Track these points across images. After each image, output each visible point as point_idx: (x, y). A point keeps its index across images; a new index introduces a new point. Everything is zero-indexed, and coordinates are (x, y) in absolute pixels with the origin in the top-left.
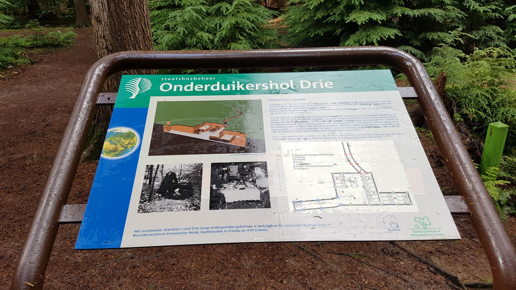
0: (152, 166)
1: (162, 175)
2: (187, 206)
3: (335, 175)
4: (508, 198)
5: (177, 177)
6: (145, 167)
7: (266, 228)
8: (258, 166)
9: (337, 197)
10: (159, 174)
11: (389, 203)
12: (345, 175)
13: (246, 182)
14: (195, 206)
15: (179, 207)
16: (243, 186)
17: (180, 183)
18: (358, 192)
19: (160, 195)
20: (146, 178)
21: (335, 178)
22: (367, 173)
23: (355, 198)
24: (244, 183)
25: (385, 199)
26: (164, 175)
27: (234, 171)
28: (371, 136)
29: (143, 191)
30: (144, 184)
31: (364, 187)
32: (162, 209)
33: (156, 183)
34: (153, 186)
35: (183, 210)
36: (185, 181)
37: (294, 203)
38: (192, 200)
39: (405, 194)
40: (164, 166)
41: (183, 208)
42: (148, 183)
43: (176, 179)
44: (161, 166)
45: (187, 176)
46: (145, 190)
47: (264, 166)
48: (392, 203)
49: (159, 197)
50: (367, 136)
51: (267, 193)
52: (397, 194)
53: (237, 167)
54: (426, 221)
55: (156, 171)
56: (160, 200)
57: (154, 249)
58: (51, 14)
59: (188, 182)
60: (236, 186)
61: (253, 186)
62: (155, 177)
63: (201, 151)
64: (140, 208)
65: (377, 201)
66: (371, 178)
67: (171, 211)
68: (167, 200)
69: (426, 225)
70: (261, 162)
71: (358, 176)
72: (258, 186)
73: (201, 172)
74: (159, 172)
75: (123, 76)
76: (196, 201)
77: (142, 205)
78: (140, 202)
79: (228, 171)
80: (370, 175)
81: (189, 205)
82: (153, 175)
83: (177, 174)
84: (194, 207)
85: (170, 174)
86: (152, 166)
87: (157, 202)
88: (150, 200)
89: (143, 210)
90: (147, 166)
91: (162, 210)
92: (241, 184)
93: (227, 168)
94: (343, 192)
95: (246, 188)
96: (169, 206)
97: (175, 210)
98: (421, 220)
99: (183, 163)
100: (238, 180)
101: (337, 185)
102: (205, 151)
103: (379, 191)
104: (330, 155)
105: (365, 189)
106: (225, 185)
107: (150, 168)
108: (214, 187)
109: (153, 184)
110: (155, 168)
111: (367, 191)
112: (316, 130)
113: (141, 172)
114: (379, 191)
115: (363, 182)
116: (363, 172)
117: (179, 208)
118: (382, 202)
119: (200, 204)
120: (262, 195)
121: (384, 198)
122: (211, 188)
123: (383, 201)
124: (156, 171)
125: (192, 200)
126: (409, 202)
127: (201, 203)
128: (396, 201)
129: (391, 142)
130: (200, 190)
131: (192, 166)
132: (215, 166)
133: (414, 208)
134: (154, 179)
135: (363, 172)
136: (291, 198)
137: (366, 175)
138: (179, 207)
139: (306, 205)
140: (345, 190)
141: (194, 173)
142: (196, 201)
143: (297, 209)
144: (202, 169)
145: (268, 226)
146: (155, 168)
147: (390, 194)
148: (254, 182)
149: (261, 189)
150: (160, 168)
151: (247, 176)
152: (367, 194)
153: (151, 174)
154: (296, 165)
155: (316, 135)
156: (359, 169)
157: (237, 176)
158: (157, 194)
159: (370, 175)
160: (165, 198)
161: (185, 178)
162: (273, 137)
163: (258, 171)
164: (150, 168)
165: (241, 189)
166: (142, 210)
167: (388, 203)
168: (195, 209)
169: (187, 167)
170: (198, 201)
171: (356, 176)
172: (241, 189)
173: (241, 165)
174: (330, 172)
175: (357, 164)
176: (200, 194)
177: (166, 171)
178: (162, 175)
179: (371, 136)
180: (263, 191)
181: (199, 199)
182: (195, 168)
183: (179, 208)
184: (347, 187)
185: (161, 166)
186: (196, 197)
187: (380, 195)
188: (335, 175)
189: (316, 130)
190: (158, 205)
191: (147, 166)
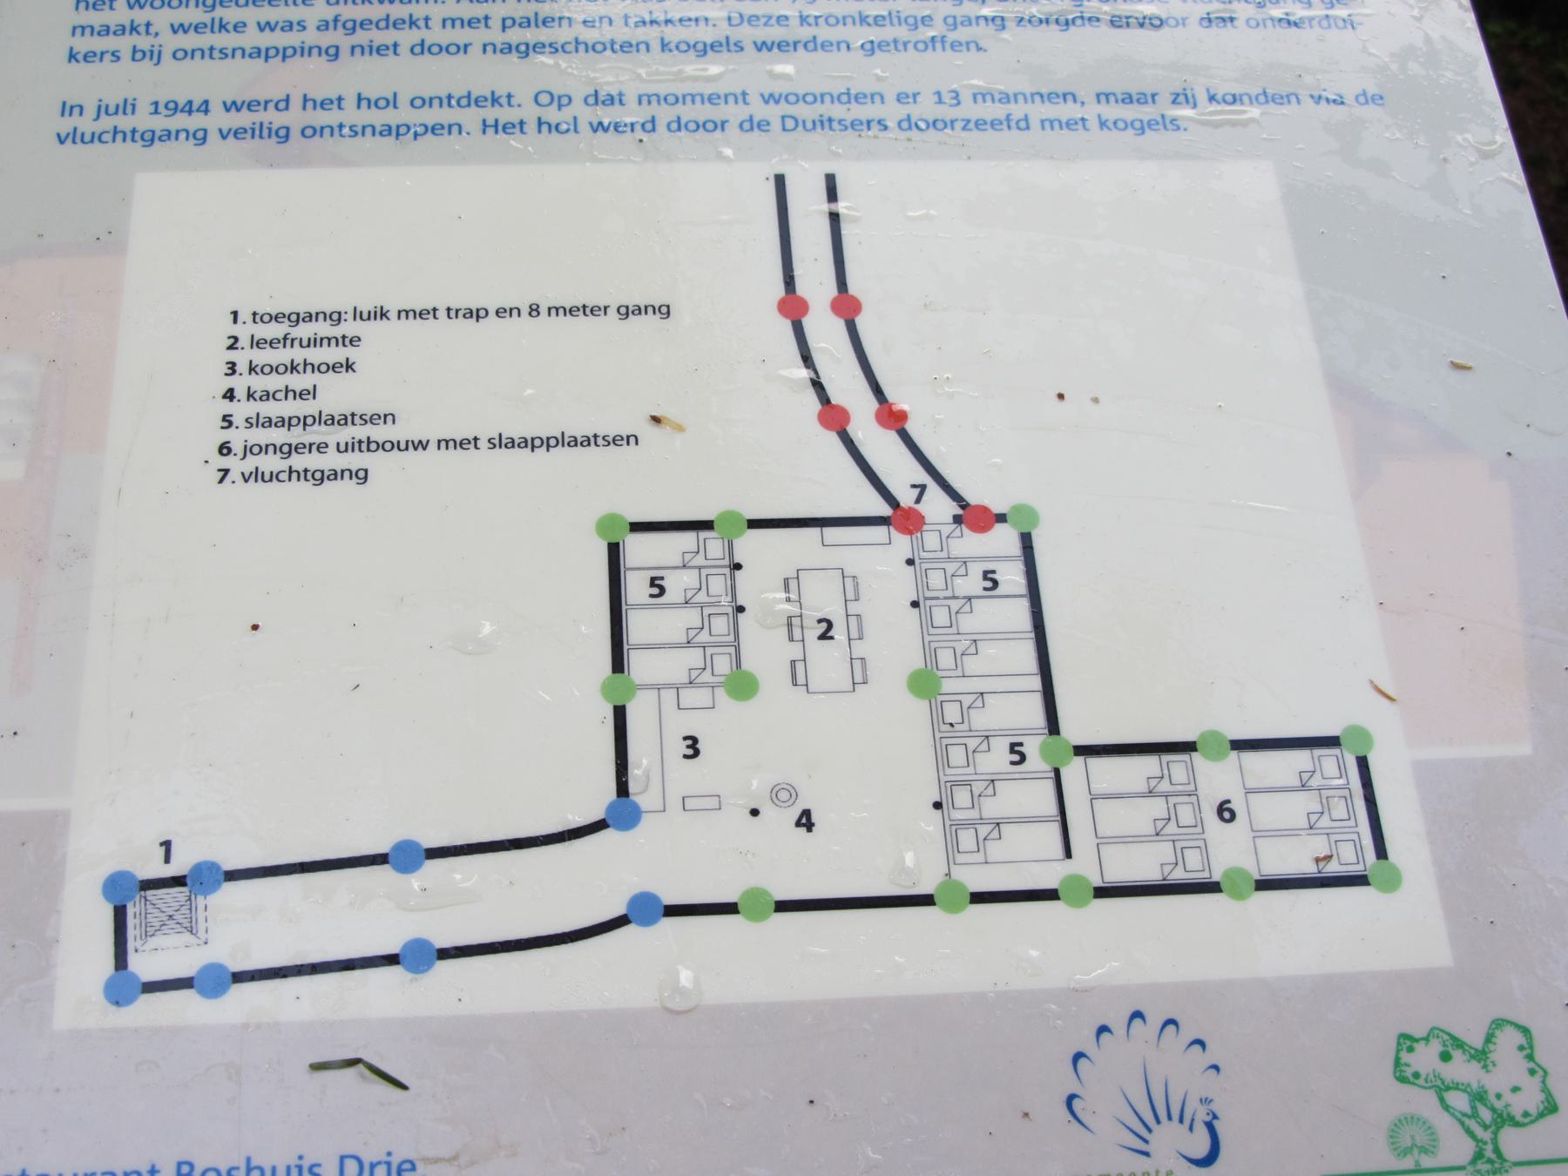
3: (641, 551)
7: (349, 328)
9: (623, 811)
11: (1151, 875)
12: (751, 545)
18: (831, 752)
21: (636, 588)
22: (974, 517)
23: (12, 1092)
25: (1123, 821)
28: (1067, 111)
31: (924, 683)
37: (126, 897)
39: (1328, 757)
48: (1192, 869)
50: (1039, 111)
52: (1251, 758)
54: (1506, 1075)
65: (1028, 856)
66: (1012, 577)
69: (1503, 1119)
71: (880, 559)
80: (1003, 539)
94: (693, 747)
98: (1461, 1070)
101: (638, 664)
103: (1075, 730)
104: (626, 312)
105: (937, 716)
111: (944, 734)
112: (531, 35)
114: (1075, 730)
115: (927, 624)
116: (937, 507)
118: (1085, 866)
121: (1115, 818)
123: (1101, 842)
126: (1352, 855)
128: (1228, 850)
129: (1252, 183)
133: (1394, 933)
135: (937, 507)
136: (114, 835)
137: (970, 543)
139: (245, 925)
140: (721, 723)
143: (145, 965)
145: (358, 315)
147: (1177, 762)
152: (942, 759)
154: (237, 438)
155: (524, 96)
156: (900, 472)
159: (1003, 539)
162: (67, 109)
167: (1143, 865)
171: (854, 561)
174: (603, 508)
175: (893, 418)
179: (1067, 111)
184: (742, 685)
187: (1074, 771)
188: (641, 551)
189: (531, 35)
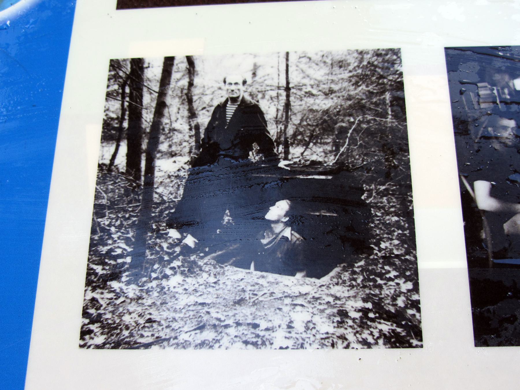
0: (138, 65)
1: (192, 114)
2: (343, 314)
5: (273, 130)
6: (105, 72)
10: (176, 115)
14: (389, 317)
15: (300, 317)
17: (296, 170)
19: (190, 241)
20: (110, 133)
26: (204, 119)
29: (99, 211)
30: (106, 171)
32: (208, 329)
33: (165, 167)
34: (150, 183)
35: (329, 342)
36: (316, 153)
38: (371, 275)
40: (199, 66)
41: (325, 326)
42: (121, 161)
43: (267, 146)
44: (181, 65)
45: (325, 126)
46: (112, 205)
49: (187, 251)
55: (162, 94)
56: (191, 269)
58: (242, 298)
59: (331, 160)
62: (156, 125)
64: (91, 314)
67: (259, 343)
68: (234, 276)
73: (399, 103)
74: (173, 103)
75: (288, 201)
76: (395, 286)
77: (104, 297)
78: (93, 281)
81: (354, 306)
82: (148, 117)
83: (270, 110)
84: (386, 327)
85: (231, 109)
86: (138, 65)
87: (175, 280)
88: (140, 268)
89: (109, 329)
90: (115, 65)
91: (208, 335)
96: (245, 313)
97: (279, 337)
99: (296, 48)
107: (128, 77)
108: (482, 190)
109: (150, 169)
110: (153, 73)
113: (84, 103)
117: (299, 326)
119: (416, 305)
122: (468, 201)
124: (162, 94)
125: (371, 275)
130: (409, 215)
131: (342, 64)
134: (154, 142)
138: (300, 317)
141: (359, 107)
142: (395, 286)
144: (400, 86)
146: (153, 73)
150: (179, 79)
153: (135, 112)
158: (174, 234)
160: (221, 261)
161: (314, 138)
164: (128, 77)
166: (103, 329)
168: (395, 341)
169: (320, 73)
170: (409, 285)
176: (410, 241)
177: (212, 90)
178: (192, 114)
181: (410, 270)
183: (299, 326)
185: (181, 65)
186: (388, 259)
190: (184, 300)
191: (115, 65)
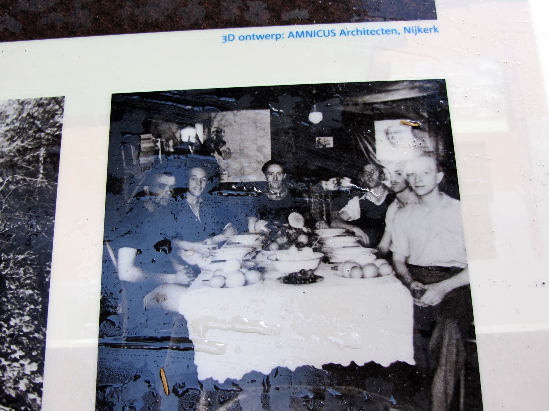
4: (384, 180)
8: (392, 112)
13: (325, 233)
16: (302, 259)
24: (312, 236)
27: (250, 139)
47: (430, 109)
51: (459, 304)
53: (264, 116)
57: (223, 25)
60: (262, 259)
61: (365, 256)
63: (58, 17)
70: (413, 84)
72: (398, 257)
73: (53, 159)
79: (211, 147)
92: (293, 241)
93: (207, 124)
95: (324, 271)
100: (274, 213)
102: (82, 17)
106: (192, 252)
119: (38, 389)
120: (426, 323)
122: (109, 268)
127: (49, 380)
130: (43, 287)
132: (136, 115)
144: (57, 140)
148: (372, 224)
149: (419, 276)
151: (329, 185)
157: (265, 186)
163: (397, 148)
165: (291, 279)
172: (291, 279)
173: (287, 102)
176: (41, 318)
180: (433, 295)
181: (36, 350)
182: (19, 132)
186: (15, 339)
